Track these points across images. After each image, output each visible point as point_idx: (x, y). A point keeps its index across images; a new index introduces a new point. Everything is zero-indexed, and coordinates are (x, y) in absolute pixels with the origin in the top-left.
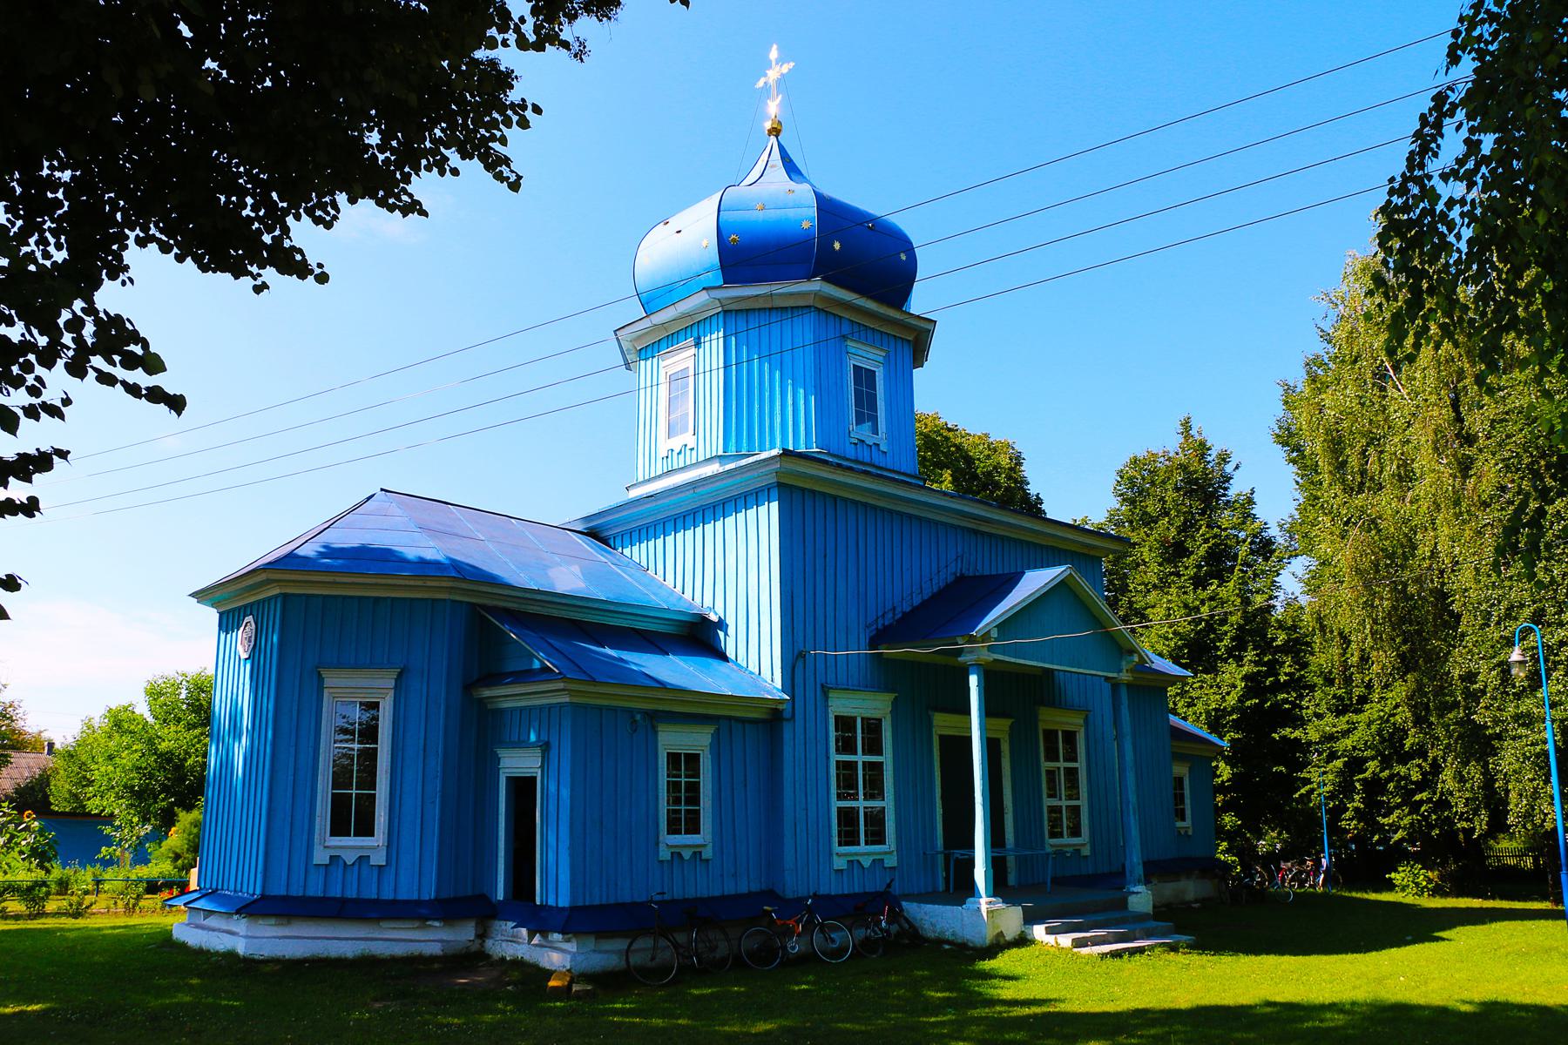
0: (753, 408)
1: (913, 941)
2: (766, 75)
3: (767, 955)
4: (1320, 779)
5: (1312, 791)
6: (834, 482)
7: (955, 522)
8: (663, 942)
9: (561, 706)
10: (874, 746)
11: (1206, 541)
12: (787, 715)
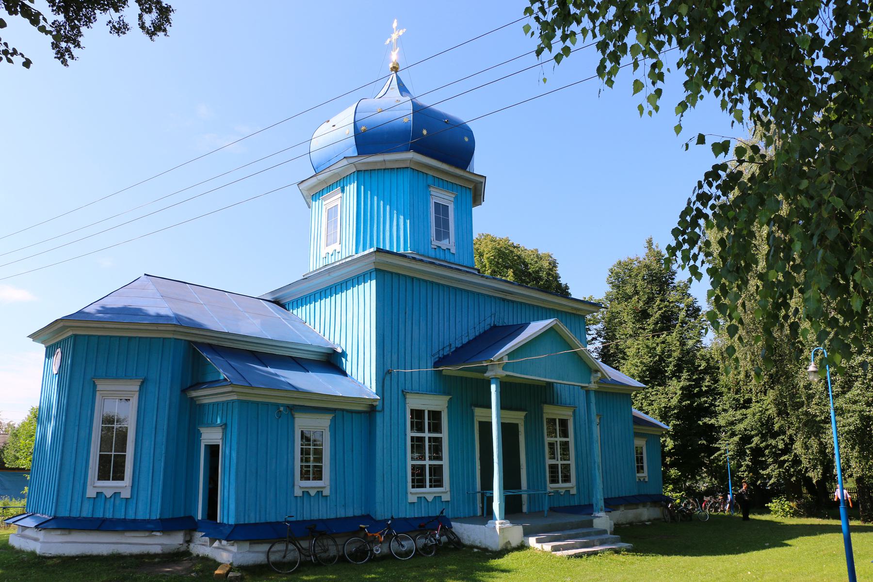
0: (373, 226)
1: (456, 546)
2: (390, 37)
3: (362, 555)
4: (727, 446)
5: (721, 455)
6: (410, 269)
7: (570, 311)
8: (291, 547)
9: (233, 401)
10: (436, 427)
11: (660, 309)
12: (379, 408)
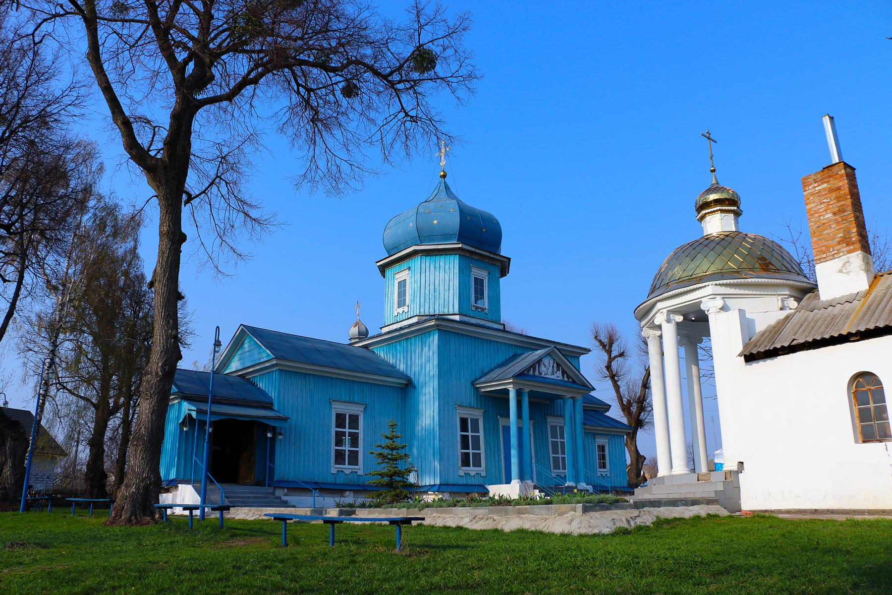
10: (476, 429)
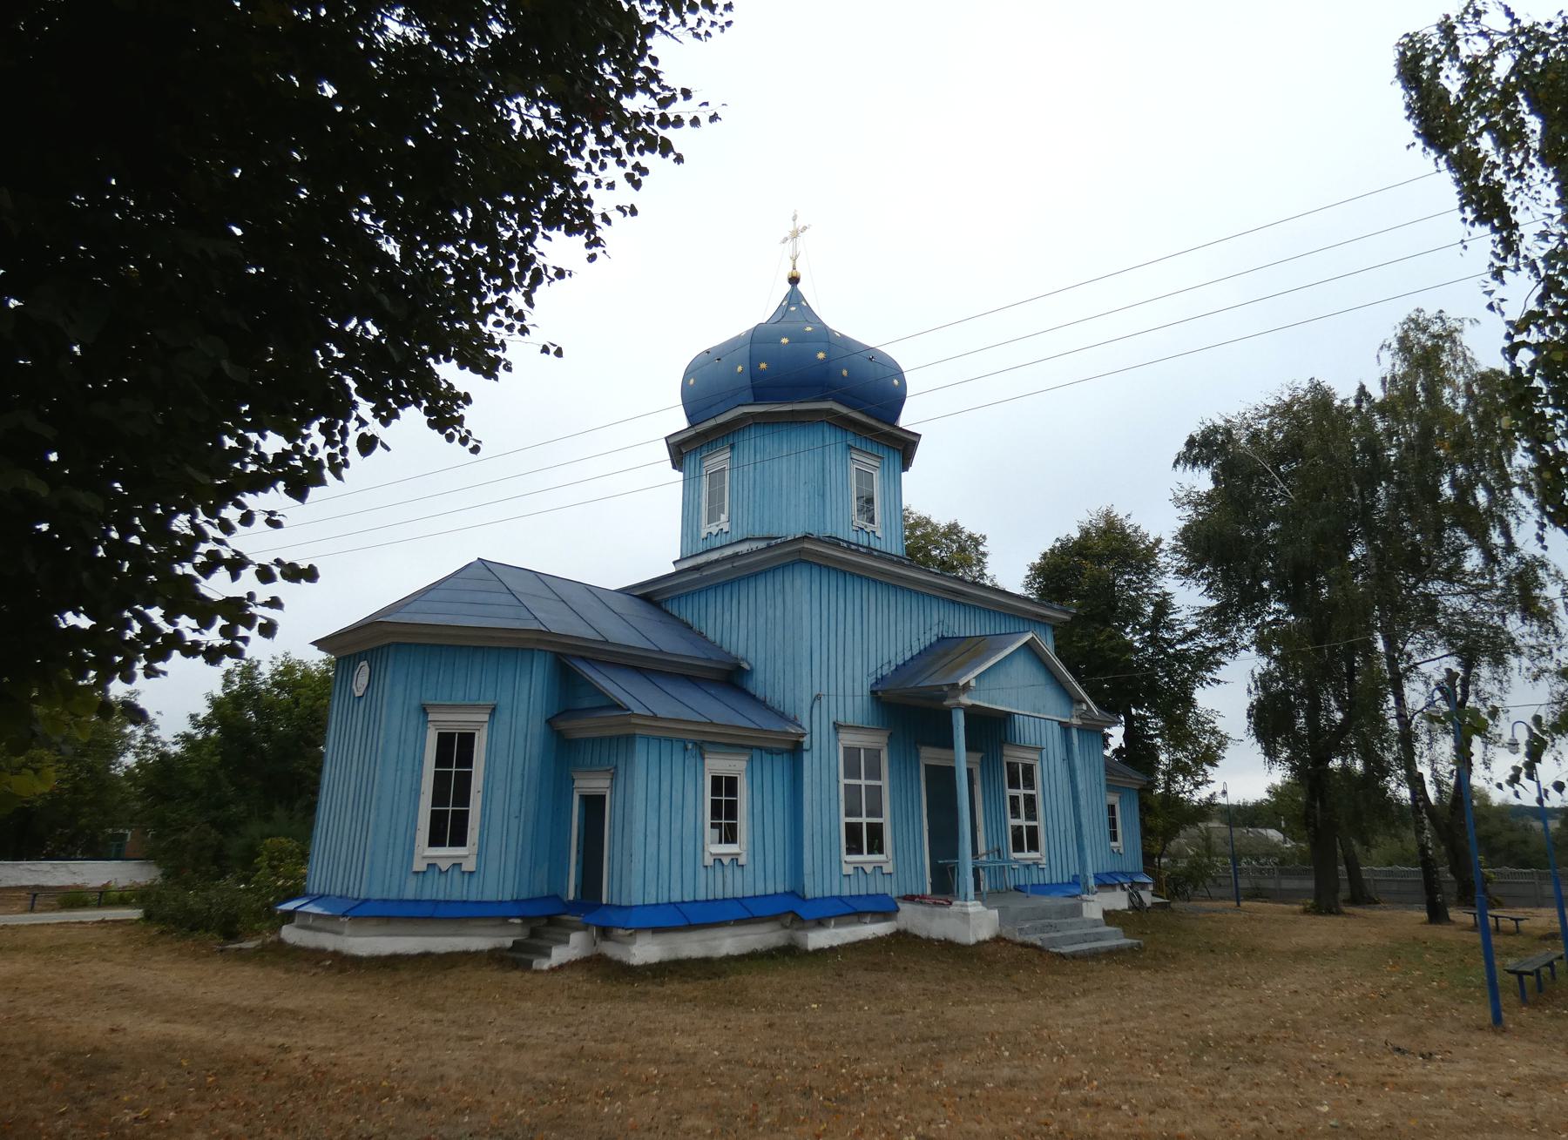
10: (874, 773)
